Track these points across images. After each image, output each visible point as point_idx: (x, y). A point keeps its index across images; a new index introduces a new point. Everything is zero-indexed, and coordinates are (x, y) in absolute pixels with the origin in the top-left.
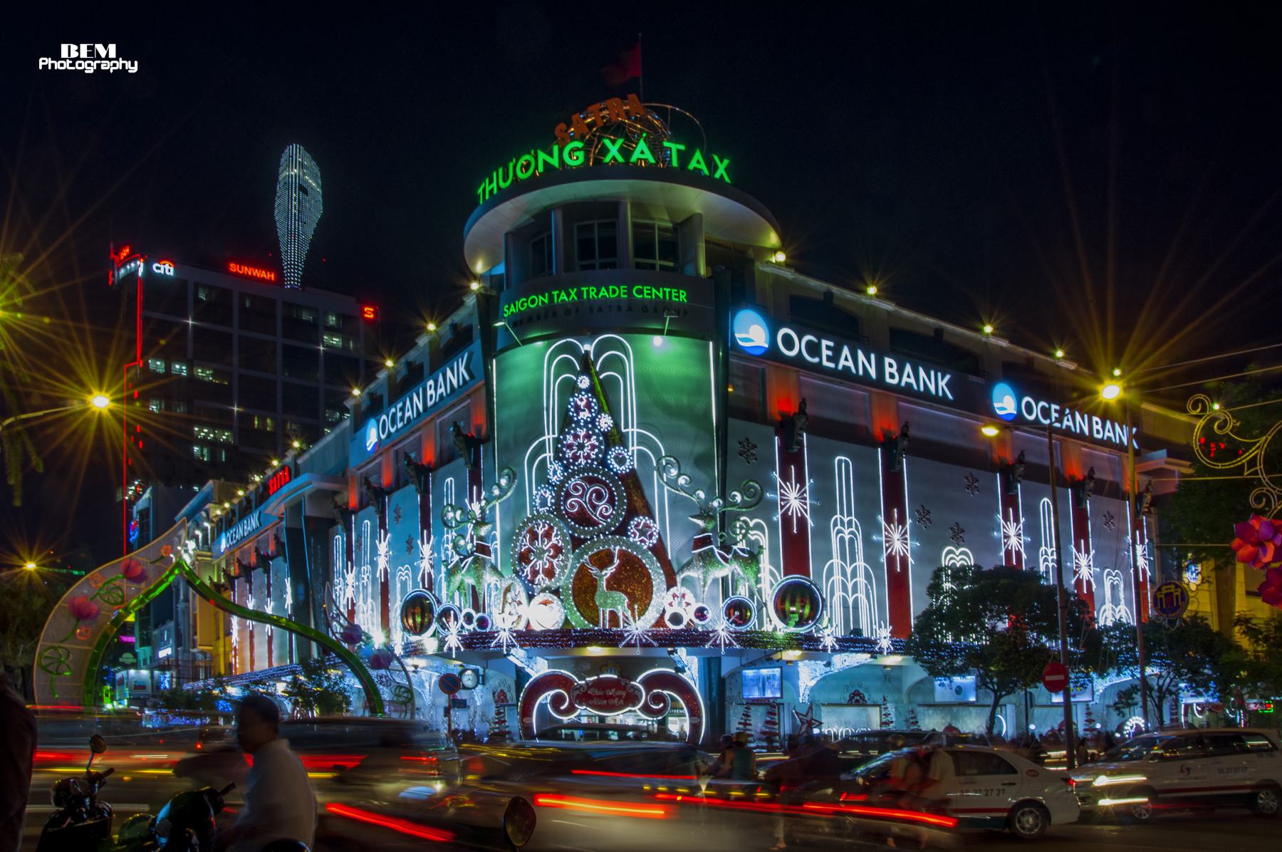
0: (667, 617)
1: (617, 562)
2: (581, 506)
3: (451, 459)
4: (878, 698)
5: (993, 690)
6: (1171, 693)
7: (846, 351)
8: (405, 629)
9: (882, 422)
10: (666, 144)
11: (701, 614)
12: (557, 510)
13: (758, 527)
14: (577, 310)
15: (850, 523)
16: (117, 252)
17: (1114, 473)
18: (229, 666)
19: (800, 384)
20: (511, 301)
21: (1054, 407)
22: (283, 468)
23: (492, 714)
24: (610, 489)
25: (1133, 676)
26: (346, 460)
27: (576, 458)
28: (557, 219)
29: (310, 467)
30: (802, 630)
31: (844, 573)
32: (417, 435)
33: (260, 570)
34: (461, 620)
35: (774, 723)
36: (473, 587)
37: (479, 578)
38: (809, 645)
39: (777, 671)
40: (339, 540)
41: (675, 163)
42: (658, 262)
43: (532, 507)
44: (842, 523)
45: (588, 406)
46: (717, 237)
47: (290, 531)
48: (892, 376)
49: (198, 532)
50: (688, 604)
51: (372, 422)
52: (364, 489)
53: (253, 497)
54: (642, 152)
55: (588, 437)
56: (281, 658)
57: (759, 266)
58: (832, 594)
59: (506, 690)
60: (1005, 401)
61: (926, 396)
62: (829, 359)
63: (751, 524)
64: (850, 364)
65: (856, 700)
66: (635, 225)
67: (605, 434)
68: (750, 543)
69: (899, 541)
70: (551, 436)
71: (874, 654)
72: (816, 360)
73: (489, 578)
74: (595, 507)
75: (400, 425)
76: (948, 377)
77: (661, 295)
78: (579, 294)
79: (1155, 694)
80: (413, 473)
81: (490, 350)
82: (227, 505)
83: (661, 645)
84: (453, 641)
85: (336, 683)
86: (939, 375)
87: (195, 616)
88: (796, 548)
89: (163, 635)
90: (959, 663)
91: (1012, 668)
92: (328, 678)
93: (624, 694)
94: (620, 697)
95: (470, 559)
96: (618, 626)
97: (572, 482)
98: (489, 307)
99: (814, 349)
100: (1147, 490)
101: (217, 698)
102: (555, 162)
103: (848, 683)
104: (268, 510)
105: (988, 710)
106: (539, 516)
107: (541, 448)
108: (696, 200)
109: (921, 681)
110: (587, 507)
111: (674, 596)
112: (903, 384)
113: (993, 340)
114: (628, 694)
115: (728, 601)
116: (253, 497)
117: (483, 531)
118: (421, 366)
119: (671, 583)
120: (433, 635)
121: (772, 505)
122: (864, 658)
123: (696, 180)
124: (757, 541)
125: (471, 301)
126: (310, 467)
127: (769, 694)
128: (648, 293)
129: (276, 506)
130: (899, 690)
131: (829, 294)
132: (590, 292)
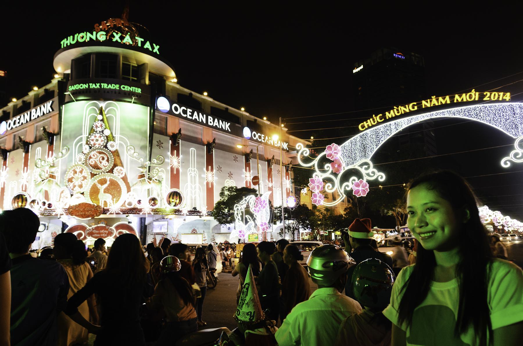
0: (126, 203)
1: (108, 183)
3: (40, 140)
4: (202, 231)
6: (297, 229)
12: (85, 163)
13: (162, 171)
15: (194, 170)
20: (73, 85)
27: (95, 144)
30: (176, 208)
31: (192, 188)
32: (25, 129)
41: (140, 45)
42: (131, 78)
43: (75, 161)
45: (101, 126)
46: (153, 71)
48: (211, 122)
51: (4, 123)
54: (127, 40)
58: (187, 195)
61: (222, 130)
62: (190, 115)
63: (160, 170)
65: (194, 232)
66: (123, 64)
67: (107, 137)
68: (159, 177)
69: (211, 176)
71: (200, 216)
74: (101, 163)
76: (229, 124)
78: (100, 86)
79: (292, 229)
81: (62, 102)
83: (123, 214)
88: (175, 177)
93: (107, 232)
94: (105, 233)
97: (93, 153)
98: (63, 85)
99: (185, 112)
100: (291, 163)
106: (78, 165)
107: (81, 139)
108: (146, 58)
111: (130, 195)
114: (109, 232)
117: (53, 170)
118: (30, 103)
119: (129, 190)
121: (168, 164)
123: (147, 51)
124: (161, 176)
128: (127, 88)
130: (209, 228)
131: (191, 94)
132: (105, 86)
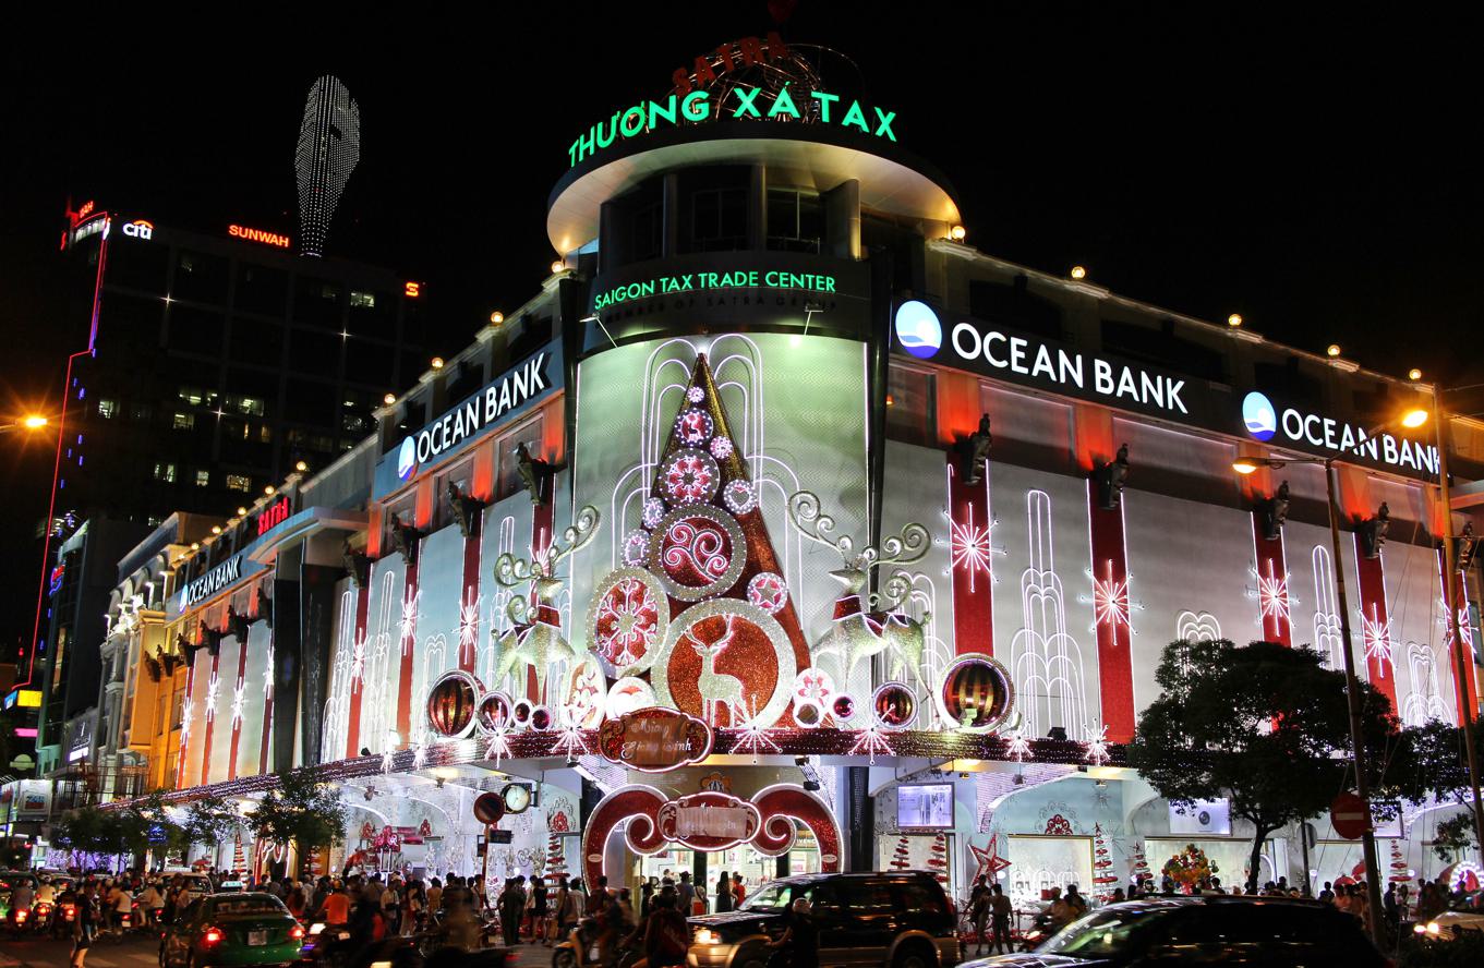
0: (796, 712)
1: (730, 634)
2: (685, 558)
3: (512, 491)
4: (1089, 827)
5: (1255, 821)
7: (1043, 352)
8: (431, 726)
9: (1090, 445)
10: (815, 94)
11: (843, 706)
14: (692, 301)
16: (77, 210)
17: (1415, 509)
18: (171, 774)
19: (981, 394)
20: (607, 288)
21: (1328, 422)
22: (280, 498)
23: (546, 844)
24: (724, 534)
25: (1460, 800)
26: (368, 489)
27: (681, 494)
28: (670, 187)
29: (317, 498)
31: (1039, 649)
32: (469, 457)
33: (233, 637)
34: (513, 715)
35: (941, 864)
36: (531, 669)
37: (541, 654)
38: (991, 749)
39: (947, 789)
40: (350, 597)
41: (826, 118)
44: (1037, 581)
45: (702, 426)
46: (875, 207)
47: (280, 584)
48: (1105, 383)
49: (151, 585)
50: (825, 692)
51: (409, 441)
52: (390, 529)
53: (233, 537)
54: (784, 105)
55: (699, 466)
56: (248, 763)
57: (933, 245)
59: (566, 812)
60: (1258, 412)
62: (1020, 362)
64: (1049, 368)
66: (771, 194)
68: (913, 607)
70: (649, 465)
72: (1003, 364)
73: (555, 654)
74: (703, 560)
75: (446, 445)
76: (1180, 384)
77: (802, 284)
78: (696, 282)
80: (459, 509)
81: (577, 349)
82: (195, 547)
83: (787, 752)
84: (499, 744)
85: (327, 802)
86: (1169, 381)
87: (130, 702)
88: (973, 609)
89: (78, 728)
90: (1204, 778)
91: (1275, 792)
92: (314, 795)
95: (530, 629)
96: (728, 724)
97: (675, 526)
98: (576, 294)
101: (147, 824)
102: (671, 116)
103: (1045, 804)
104: (253, 556)
105: (1249, 848)
108: (849, 163)
109: (1150, 803)
110: (694, 561)
111: (807, 681)
112: (1119, 394)
113: (1243, 335)
115: (880, 690)
116: (233, 537)
117: (550, 591)
118: (480, 369)
119: (803, 663)
120: (471, 735)
122: (1070, 770)
125: (551, 287)
126: (317, 498)
127: (934, 822)
128: (786, 281)
129: (265, 551)
130: (1119, 815)
131: (1022, 279)
